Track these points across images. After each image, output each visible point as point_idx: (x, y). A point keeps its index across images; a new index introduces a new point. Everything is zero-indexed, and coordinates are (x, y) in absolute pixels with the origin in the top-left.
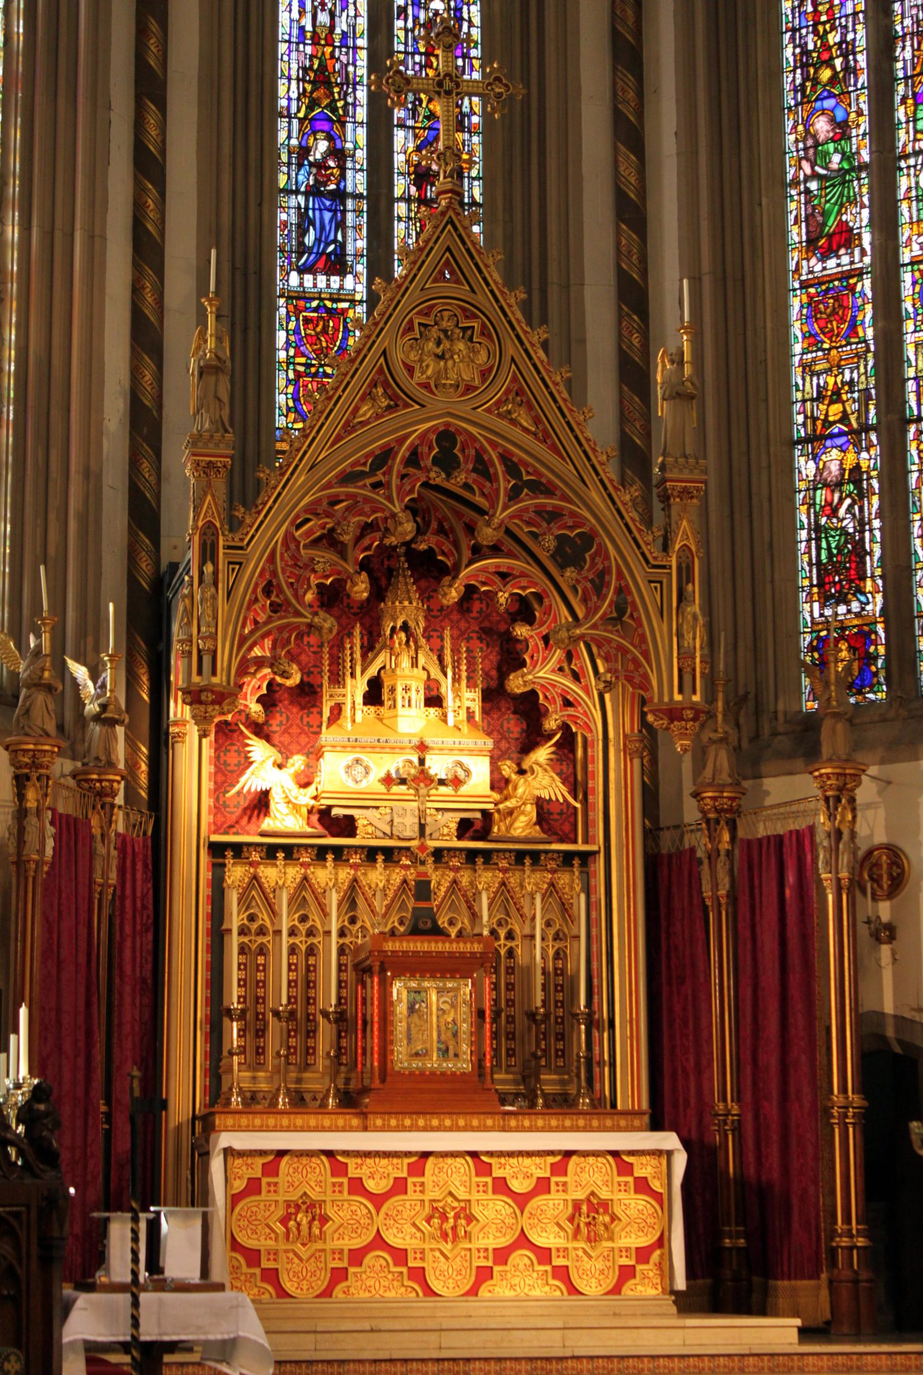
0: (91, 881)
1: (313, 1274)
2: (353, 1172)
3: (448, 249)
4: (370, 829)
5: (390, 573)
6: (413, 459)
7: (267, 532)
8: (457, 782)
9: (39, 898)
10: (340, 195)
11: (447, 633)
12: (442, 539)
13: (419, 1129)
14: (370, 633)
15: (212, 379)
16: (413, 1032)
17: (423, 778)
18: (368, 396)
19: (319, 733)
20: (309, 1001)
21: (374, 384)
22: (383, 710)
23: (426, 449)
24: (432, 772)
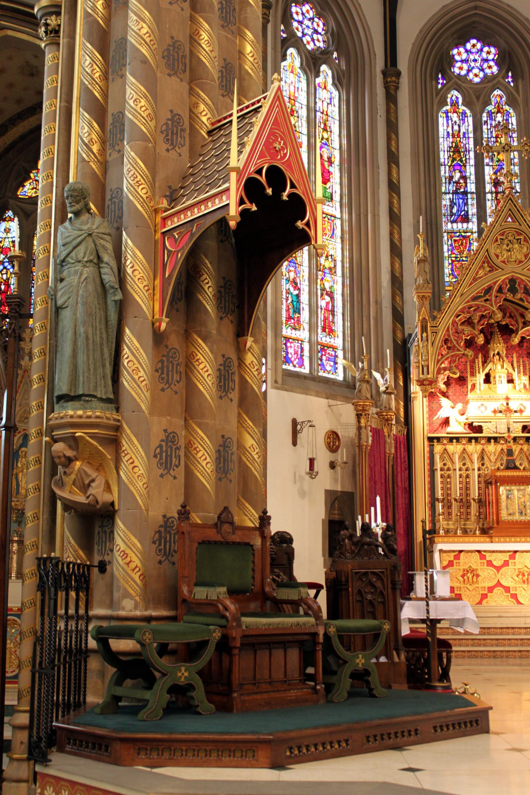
0: (385, 452)
1: (474, 596)
2: (488, 558)
3: (510, 210)
4: (488, 430)
5: (492, 333)
6: (500, 290)
7: (446, 321)
8: (521, 411)
9: (367, 459)
10: (465, 193)
11: (515, 355)
12: (511, 319)
13: (512, 542)
14: (485, 357)
15: (422, 264)
16: (509, 505)
17: (508, 410)
18: (482, 267)
19: (467, 395)
20: (467, 495)
21: (484, 262)
22: (491, 385)
23: (505, 286)
24: (511, 408)
